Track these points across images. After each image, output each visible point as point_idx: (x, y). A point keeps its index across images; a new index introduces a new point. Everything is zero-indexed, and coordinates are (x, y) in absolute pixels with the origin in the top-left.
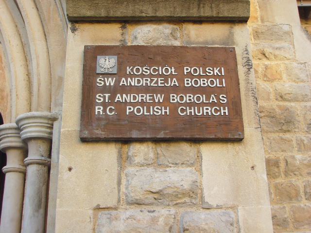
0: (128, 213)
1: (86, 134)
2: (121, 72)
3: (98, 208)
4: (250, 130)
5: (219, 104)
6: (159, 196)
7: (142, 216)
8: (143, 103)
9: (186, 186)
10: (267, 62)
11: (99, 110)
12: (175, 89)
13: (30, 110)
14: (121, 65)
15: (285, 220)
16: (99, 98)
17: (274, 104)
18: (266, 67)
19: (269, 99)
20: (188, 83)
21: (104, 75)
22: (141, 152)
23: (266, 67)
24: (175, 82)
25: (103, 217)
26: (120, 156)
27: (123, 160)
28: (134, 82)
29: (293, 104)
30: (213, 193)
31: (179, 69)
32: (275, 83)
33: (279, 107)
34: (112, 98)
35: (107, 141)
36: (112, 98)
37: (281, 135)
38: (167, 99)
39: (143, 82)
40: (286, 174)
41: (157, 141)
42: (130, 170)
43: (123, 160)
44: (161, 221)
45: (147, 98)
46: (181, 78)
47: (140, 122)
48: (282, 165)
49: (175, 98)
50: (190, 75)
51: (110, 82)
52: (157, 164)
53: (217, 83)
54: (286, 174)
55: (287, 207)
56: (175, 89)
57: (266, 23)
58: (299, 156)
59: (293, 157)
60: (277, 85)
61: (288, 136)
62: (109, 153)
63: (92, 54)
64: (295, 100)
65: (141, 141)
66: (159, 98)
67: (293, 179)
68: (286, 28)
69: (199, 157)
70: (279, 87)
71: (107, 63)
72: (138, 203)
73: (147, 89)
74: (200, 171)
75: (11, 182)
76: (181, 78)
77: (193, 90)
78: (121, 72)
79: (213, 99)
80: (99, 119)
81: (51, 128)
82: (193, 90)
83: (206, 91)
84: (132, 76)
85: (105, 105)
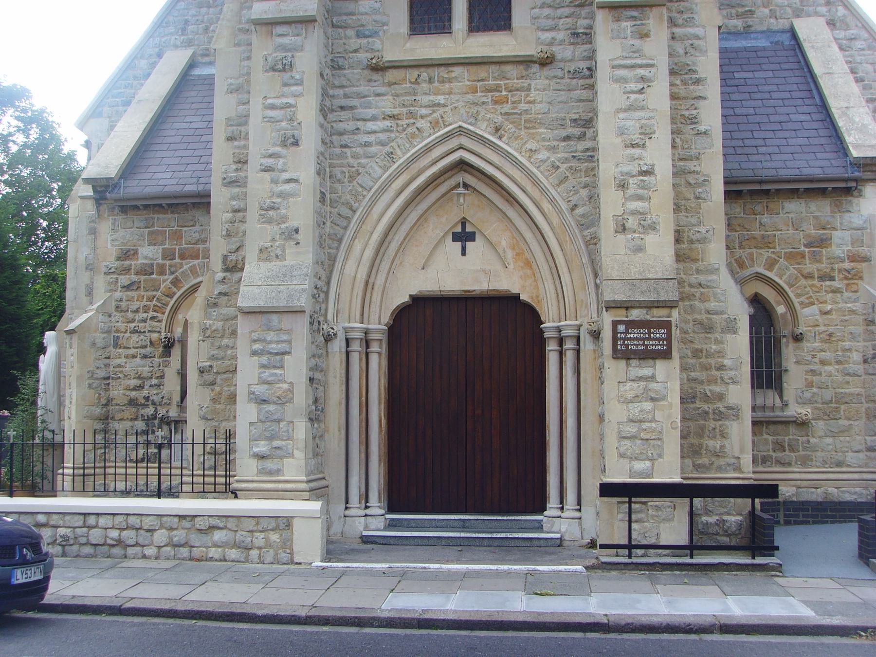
0: (630, 384)
1: (615, 356)
2: (627, 332)
3: (619, 382)
4: (675, 354)
5: (663, 345)
6: (641, 379)
7: (635, 385)
8: (635, 345)
9: (650, 375)
10: (702, 290)
11: (619, 347)
12: (647, 339)
13: (560, 322)
14: (627, 329)
15: (702, 381)
16: (619, 342)
17: (704, 317)
18: (702, 294)
19: (701, 313)
20: (652, 336)
21: (620, 333)
22: (634, 362)
23: (702, 294)
24: (647, 336)
25: (621, 385)
26: (627, 364)
27: (628, 365)
28: (631, 336)
29: (714, 316)
30: (659, 378)
31: (649, 331)
32: (705, 303)
33: (707, 318)
34: (624, 342)
35: (622, 358)
36: (624, 342)
37: (706, 335)
38: (644, 342)
39: (636, 336)
40: (706, 357)
41: (640, 359)
42: (630, 368)
43: (628, 365)
44: (641, 387)
45: (637, 342)
46: (649, 334)
47: (635, 352)
48: (705, 352)
49: (647, 342)
50: (653, 333)
51: (623, 336)
52: (640, 366)
53: (663, 336)
54: (706, 357)
55: (705, 374)
56: (647, 339)
57: (704, 263)
58: (714, 347)
59: (711, 348)
60: (707, 305)
61: (709, 335)
62: (622, 363)
63: (615, 324)
64: (716, 313)
65: (634, 358)
66: (641, 342)
67: (709, 360)
68: (716, 266)
69: (655, 364)
70: (707, 306)
71: (621, 328)
72: (633, 380)
73: (636, 339)
74: (655, 369)
75: (552, 360)
76: (649, 334)
77: (654, 339)
78: (627, 332)
79: (661, 343)
80: (619, 350)
81: (579, 330)
82: (654, 339)
83: (659, 339)
84: (631, 333)
85: (621, 345)
